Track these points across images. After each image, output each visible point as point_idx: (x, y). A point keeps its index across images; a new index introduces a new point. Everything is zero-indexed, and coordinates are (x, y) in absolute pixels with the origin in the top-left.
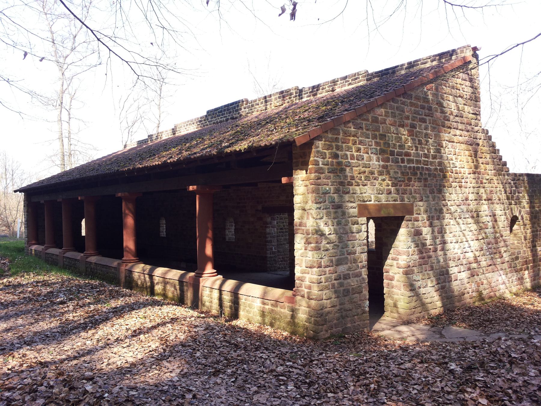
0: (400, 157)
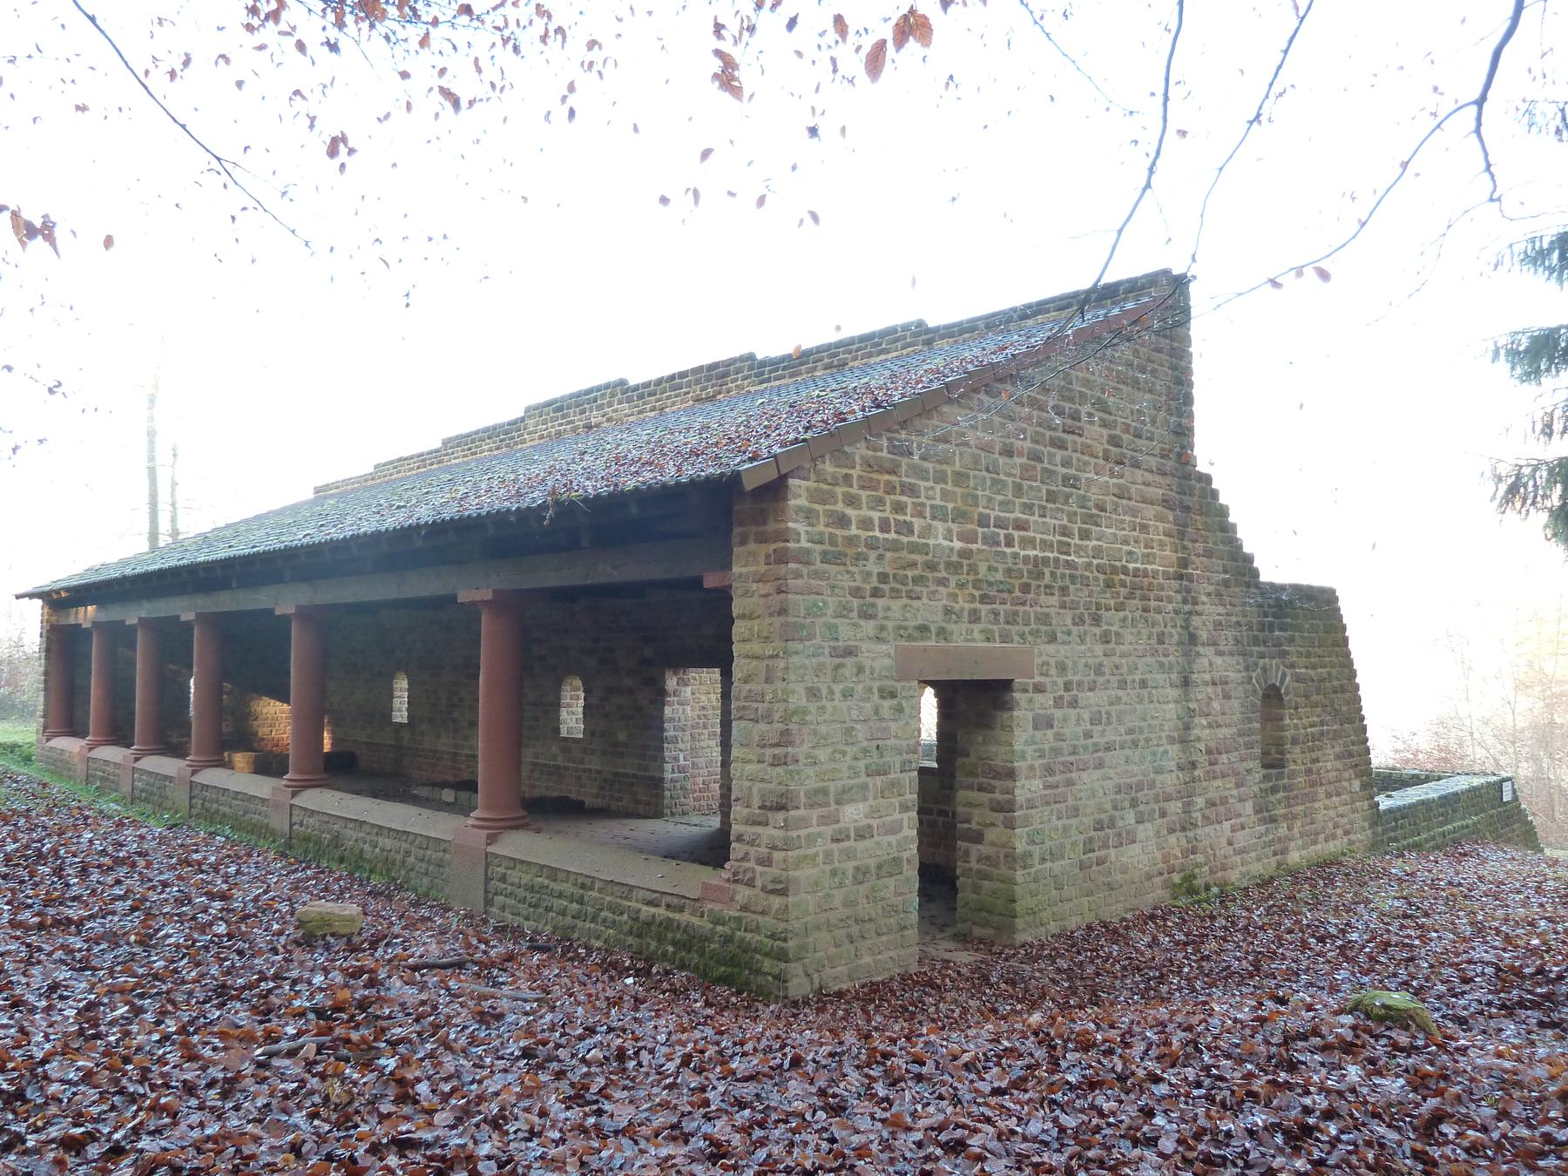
0: (1002, 532)
